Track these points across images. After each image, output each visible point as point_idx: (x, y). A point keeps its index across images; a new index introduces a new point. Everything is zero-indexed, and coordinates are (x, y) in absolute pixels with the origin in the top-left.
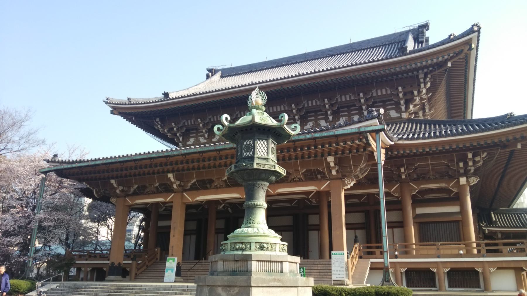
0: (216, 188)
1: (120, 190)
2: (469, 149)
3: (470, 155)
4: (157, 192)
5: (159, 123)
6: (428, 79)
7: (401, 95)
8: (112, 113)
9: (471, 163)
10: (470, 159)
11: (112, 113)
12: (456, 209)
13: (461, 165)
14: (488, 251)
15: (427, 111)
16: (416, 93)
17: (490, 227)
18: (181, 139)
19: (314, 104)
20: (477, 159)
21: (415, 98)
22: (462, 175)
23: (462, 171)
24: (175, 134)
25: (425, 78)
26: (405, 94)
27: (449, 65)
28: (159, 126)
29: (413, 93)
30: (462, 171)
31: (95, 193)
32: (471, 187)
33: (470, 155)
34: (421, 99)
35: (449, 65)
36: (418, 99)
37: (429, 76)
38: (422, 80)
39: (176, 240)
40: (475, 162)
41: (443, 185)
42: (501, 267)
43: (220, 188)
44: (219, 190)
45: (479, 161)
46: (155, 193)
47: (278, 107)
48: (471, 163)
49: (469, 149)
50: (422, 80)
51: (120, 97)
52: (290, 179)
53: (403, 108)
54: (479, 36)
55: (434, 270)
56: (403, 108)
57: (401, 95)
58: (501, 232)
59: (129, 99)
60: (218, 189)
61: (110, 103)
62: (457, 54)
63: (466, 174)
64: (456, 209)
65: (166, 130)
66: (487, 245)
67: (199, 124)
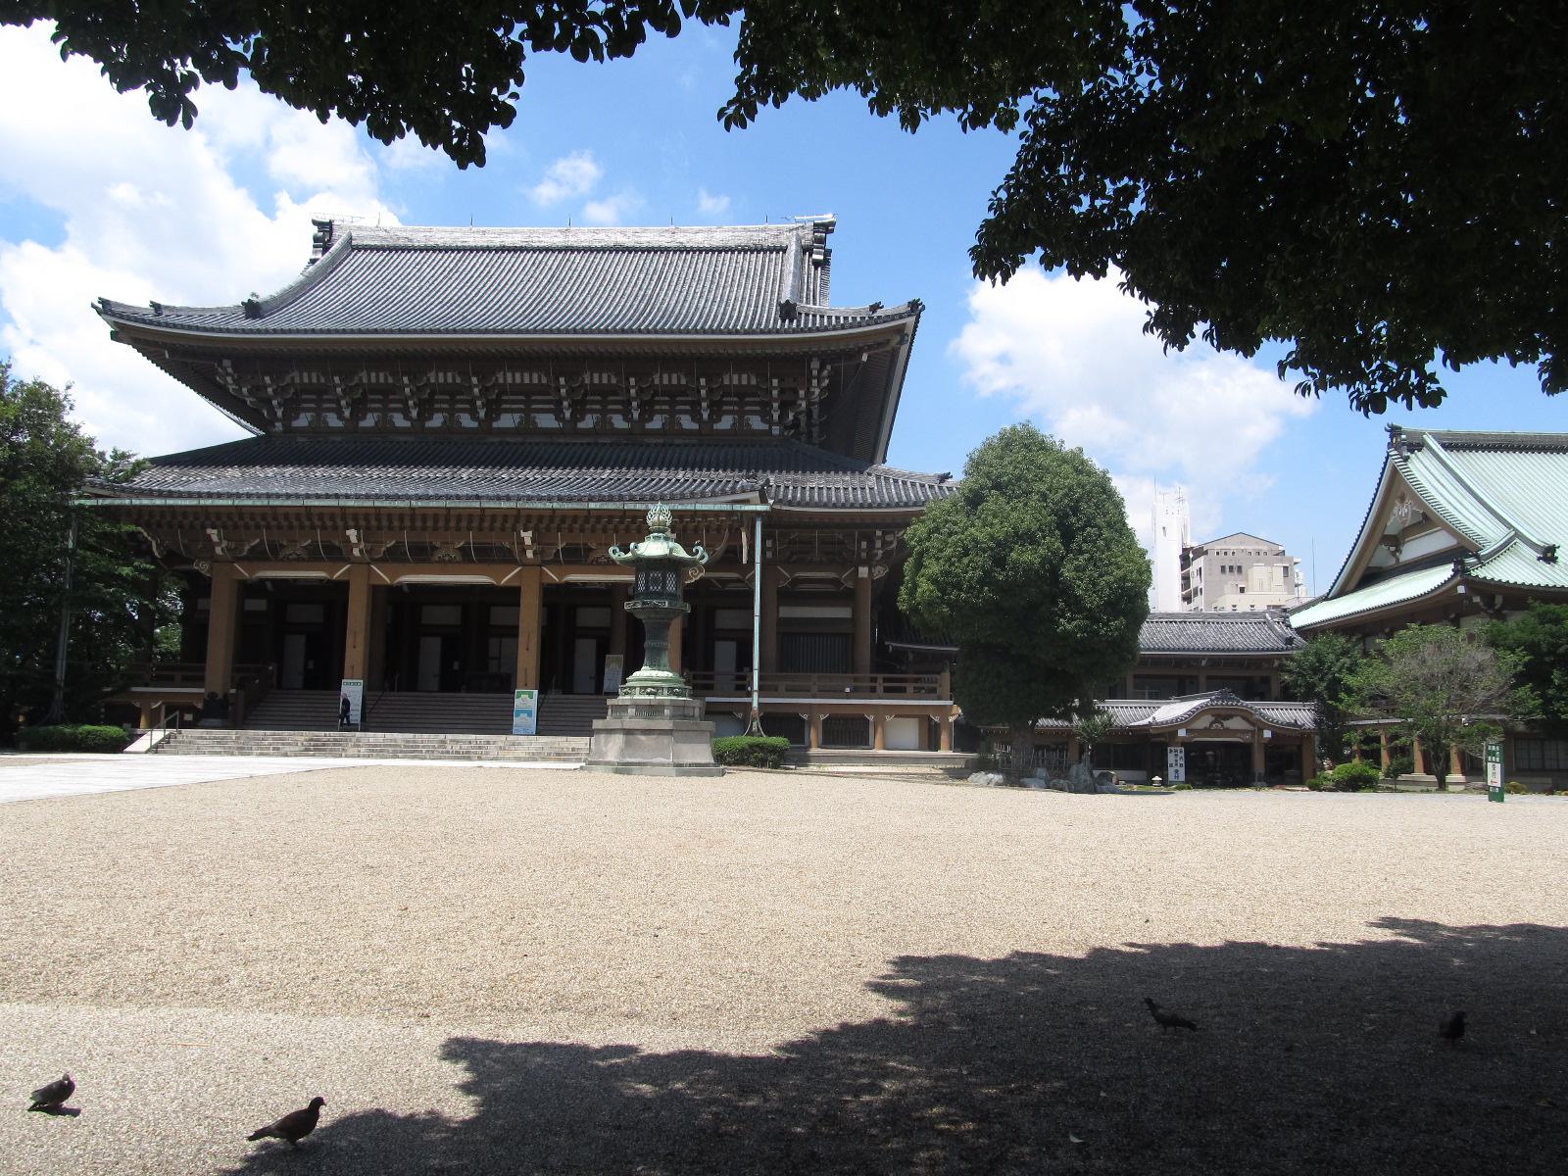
0: (441, 561)
1: (223, 550)
2: (878, 526)
3: (879, 533)
4: (313, 557)
5: (230, 370)
6: (825, 373)
7: (775, 393)
8: (115, 336)
9: (878, 544)
10: (879, 538)
11: (115, 336)
12: (844, 613)
13: (864, 545)
14: (887, 690)
15: (815, 435)
16: (802, 393)
17: (896, 641)
18: (280, 413)
19: (605, 381)
20: (889, 538)
21: (799, 402)
22: (863, 563)
23: (864, 555)
24: (269, 401)
25: (820, 371)
26: (782, 391)
27: (865, 358)
28: (229, 379)
29: (796, 392)
30: (864, 555)
31: (154, 549)
32: (873, 581)
33: (879, 533)
34: (810, 404)
35: (865, 358)
36: (804, 404)
37: (829, 367)
38: (815, 373)
39: (356, 651)
40: (885, 543)
41: (832, 575)
42: (902, 713)
43: (450, 562)
44: (449, 565)
45: (891, 543)
46: (303, 560)
47: (526, 375)
48: (878, 544)
49: (878, 526)
50: (815, 373)
51: (136, 296)
52: (589, 561)
53: (776, 416)
54: (917, 322)
55: (805, 717)
56: (776, 416)
57: (775, 393)
58: (913, 651)
59: (156, 307)
60: (445, 566)
61: (113, 314)
62: (880, 345)
63: (868, 562)
64: (844, 613)
65: (245, 390)
66: (885, 680)
67: (335, 387)
